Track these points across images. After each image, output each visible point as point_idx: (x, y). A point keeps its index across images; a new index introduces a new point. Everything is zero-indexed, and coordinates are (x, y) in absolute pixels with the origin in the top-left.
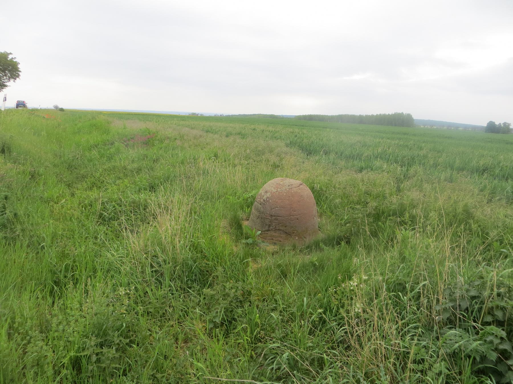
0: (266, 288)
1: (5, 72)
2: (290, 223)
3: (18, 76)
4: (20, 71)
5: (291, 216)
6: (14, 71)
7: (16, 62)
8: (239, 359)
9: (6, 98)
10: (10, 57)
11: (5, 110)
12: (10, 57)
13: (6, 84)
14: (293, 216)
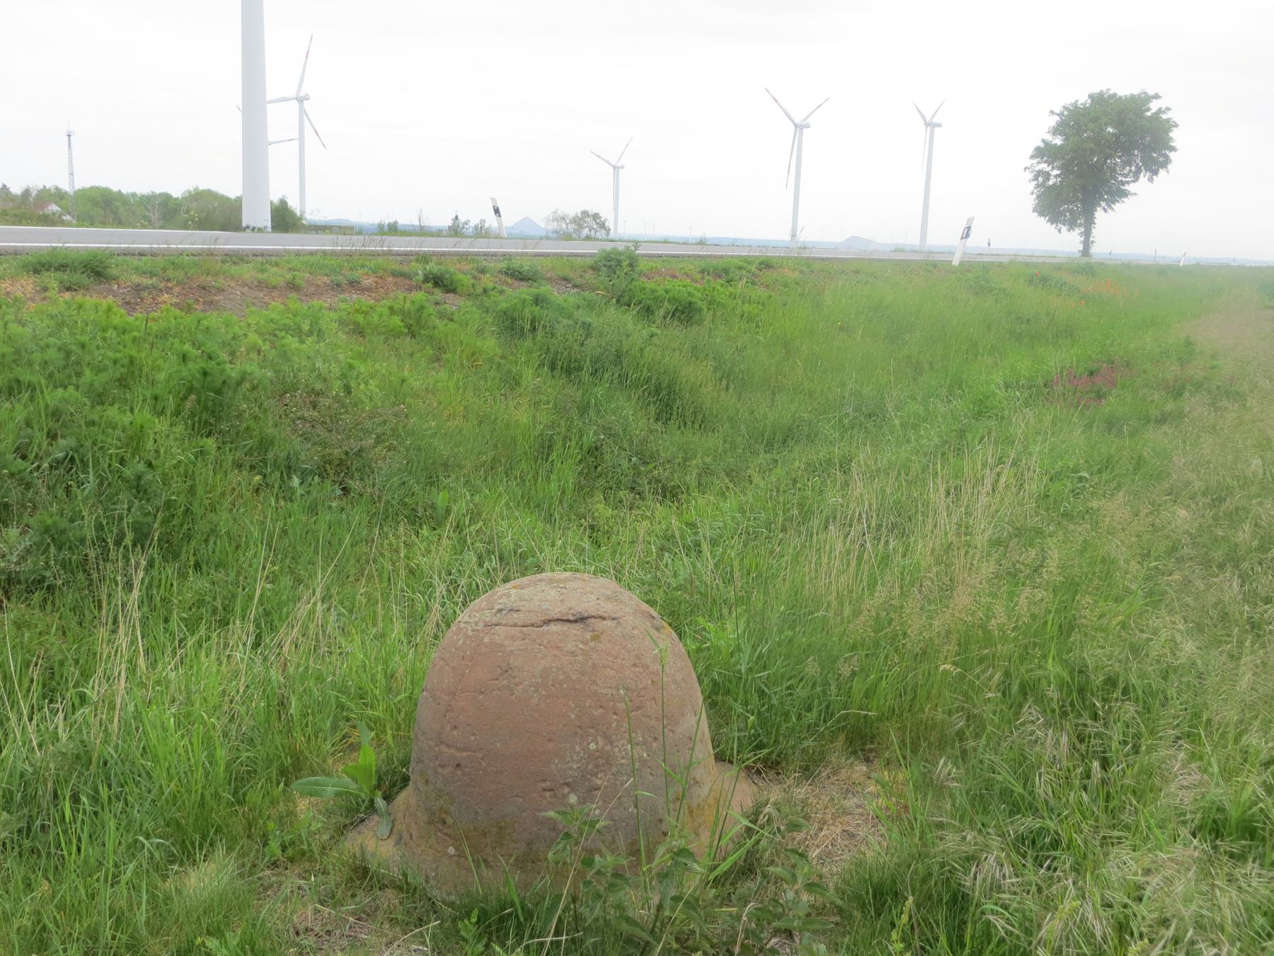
0: (262, 943)
3: (1165, 163)
4: (1173, 149)
7: (1168, 121)
9: (969, 228)
10: (1154, 106)
11: (961, 263)
12: (1154, 106)
13: (1127, 187)
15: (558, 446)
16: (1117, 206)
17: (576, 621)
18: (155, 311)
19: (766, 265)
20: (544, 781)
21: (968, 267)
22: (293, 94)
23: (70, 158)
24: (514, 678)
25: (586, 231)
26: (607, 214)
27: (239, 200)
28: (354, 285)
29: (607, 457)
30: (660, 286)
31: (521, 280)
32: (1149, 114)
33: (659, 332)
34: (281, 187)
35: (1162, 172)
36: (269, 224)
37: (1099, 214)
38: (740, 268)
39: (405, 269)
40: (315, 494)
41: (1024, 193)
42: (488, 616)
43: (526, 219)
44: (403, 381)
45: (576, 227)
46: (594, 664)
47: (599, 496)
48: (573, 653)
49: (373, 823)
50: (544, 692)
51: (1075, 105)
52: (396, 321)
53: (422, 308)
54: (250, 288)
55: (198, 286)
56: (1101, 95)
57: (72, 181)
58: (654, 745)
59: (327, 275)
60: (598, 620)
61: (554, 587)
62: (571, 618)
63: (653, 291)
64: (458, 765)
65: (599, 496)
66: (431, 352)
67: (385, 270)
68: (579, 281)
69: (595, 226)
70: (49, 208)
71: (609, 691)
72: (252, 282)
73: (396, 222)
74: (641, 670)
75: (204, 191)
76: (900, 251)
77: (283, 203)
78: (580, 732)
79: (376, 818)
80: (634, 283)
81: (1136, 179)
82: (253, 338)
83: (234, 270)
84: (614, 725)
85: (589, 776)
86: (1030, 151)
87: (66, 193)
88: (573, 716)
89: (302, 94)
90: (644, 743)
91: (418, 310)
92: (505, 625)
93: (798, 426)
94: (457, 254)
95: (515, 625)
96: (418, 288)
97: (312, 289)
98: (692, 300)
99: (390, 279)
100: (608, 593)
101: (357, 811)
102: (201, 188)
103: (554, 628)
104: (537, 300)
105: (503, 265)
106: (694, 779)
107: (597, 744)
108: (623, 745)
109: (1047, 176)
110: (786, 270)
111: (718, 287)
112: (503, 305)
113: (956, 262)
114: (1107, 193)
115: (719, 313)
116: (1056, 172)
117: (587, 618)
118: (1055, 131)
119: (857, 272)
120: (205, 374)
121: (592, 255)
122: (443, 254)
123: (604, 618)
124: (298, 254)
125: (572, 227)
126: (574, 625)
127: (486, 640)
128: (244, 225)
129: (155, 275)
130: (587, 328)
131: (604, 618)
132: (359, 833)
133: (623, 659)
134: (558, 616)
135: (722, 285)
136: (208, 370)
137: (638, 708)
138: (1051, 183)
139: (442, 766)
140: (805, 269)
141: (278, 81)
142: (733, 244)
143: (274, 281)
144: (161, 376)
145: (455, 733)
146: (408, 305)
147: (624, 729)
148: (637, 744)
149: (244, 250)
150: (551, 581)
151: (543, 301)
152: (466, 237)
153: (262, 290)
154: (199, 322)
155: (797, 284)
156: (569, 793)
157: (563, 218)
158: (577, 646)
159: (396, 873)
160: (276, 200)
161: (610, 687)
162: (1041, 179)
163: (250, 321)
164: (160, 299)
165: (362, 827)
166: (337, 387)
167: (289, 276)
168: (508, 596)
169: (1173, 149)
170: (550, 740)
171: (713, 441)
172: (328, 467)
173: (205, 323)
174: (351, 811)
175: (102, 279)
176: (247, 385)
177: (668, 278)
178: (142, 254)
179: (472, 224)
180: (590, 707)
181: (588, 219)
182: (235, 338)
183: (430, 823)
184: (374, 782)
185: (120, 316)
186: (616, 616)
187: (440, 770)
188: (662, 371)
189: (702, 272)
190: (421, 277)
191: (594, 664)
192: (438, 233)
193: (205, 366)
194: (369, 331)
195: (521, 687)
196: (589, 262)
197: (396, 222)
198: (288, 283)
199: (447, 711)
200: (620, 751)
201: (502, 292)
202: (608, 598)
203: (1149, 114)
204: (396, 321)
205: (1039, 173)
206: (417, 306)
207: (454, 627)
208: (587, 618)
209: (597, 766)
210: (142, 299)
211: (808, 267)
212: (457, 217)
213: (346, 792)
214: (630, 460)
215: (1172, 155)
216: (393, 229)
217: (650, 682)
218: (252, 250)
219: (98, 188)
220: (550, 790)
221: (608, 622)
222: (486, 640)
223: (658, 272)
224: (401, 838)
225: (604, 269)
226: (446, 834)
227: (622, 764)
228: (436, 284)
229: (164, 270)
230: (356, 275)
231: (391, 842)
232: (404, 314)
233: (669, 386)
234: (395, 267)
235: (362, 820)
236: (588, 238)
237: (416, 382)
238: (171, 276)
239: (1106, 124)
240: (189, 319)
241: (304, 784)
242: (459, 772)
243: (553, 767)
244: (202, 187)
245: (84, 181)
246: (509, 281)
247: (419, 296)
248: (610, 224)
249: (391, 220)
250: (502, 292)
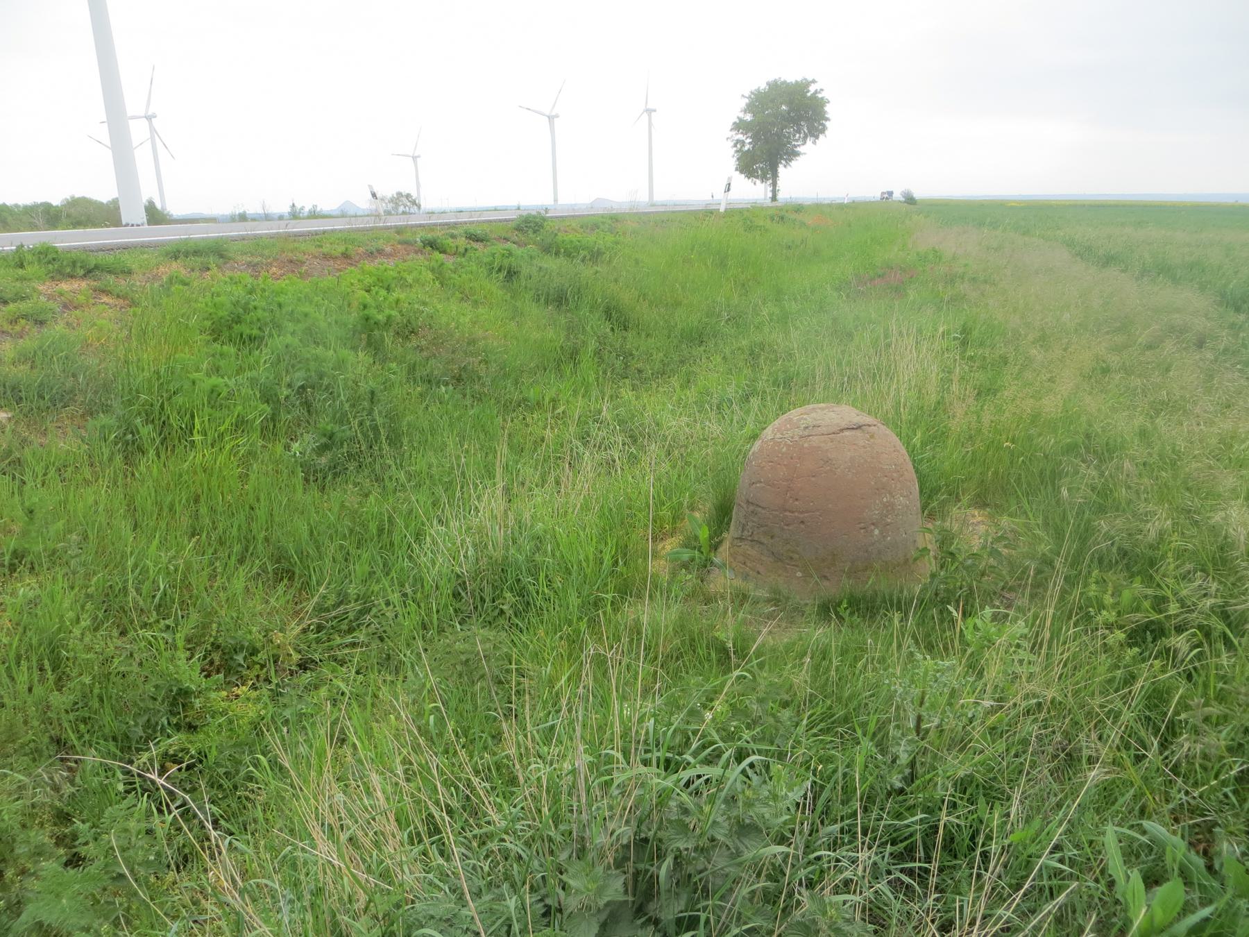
1: (799, 125)
2: (783, 529)
3: (823, 131)
4: (827, 119)
5: (785, 511)
6: (815, 120)
7: (822, 98)
8: (1084, 761)
10: (812, 89)
12: (812, 89)
13: (798, 149)
14: (793, 512)
16: (793, 163)
22: (143, 114)
25: (401, 209)
27: (115, 202)
28: (380, 252)
32: (809, 94)
34: (148, 191)
35: (821, 136)
36: (145, 220)
37: (781, 169)
41: (727, 161)
51: (758, 90)
53: (442, 264)
56: (775, 81)
81: (805, 143)
86: (730, 126)
89: (150, 113)
102: (77, 196)
103: (847, 433)
109: (743, 143)
113: (722, 210)
114: (785, 154)
116: (749, 140)
118: (745, 111)
125: (390, 206)
128: (124, 223)
131: (869, 426)
138: (746, 148)
141: (133, 104)
142: (472, 212)
145: (797, 503)
152: (300, 219)
162: (739, 146)
169: (827, 119)
179: (307, 209)
196: (513, 224)
198: (342, 254)
203: (809, 94)
205: (738, 141)
206: (439, 263)
212: (293, 205)
215: (827, 124)
216: (243, 218)
239: (781, 104)
242: (802, 526)
249: (241, 211)
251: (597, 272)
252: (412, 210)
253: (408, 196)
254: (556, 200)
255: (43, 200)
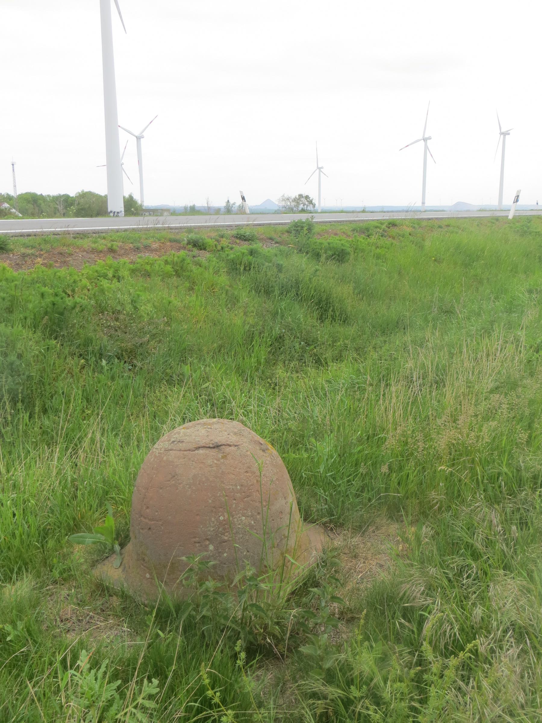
9: (518, 196)
11: (514, 217)
15: (256, 338)
17: (214, 448)
18: (33, 268)
19: (393, 224)
20: (195, 537)
21: (517, 219)
23: (14, 177)
24: (178, 480)
25: (301, 206)
26: (314, 196)
27: (106, 196)
28: (147, 248)
29: (287, 342)
30: (324, 241)
31: (245, 240)
33: (320, 268)
36: (123, 210)
38: (377, 227)
39: (178, 237)
40: (115, 369)
42: (167, 445)
43: (268, 200)
44: (170, 303)
45: (295, 204)
46: (222, 472)
47: (281, 364)
48: (211, 466)
49: (112, 559)
50: (194, 488)
52: (169, 268)
54: (87, 252)
55: (58, 253)
57: (16, 192)
58: (258, 517)
59: (132, 243)
60: (227, 447)
61: (205, 428)
62: (211, 446)
63: (321, 244)
64: (150, 529)
65: (281, 364)
66: (188, 285)
67: (165, 239)
68: (279, 240)
69: (307, 203)
70: (4, 205)
71: (231, 487)
72: (89, 249)
73: (194, 206)
74: (250, 475)
75: (87, 192)
76: (485, 210)
77: (131, 197)
78: (214, 510)
79: (115, 556)
80: (310, 240)
82: (85, 282)
83: (80, 242)
84: (234, 506)
85: (220, 535)
87: (13, 196)
88: (210, 501)
90: (252, 516)
91: (181, 261)
92: (175, 450)
93: (402, 320)
94: (208, 227)
95: (180, 450)
96: (184, 248)
97: (123, 251)
98: (344, 248)
99: (168, 244)
100: (236, 430)
101: (104, 552)
103: (201, 451)
104: (252, 253)
105: (234, 232)
106: (284, 535)
107: (224, 516)
108: (239, 517)
110: (405, 227)
111: (361, 240)
112: (232, 256)
113: (510, 217)
115: (360, 255)
117: (220, 446)
119: (448, 226)
120: (54, 304)
121: (285, 224)
122: (200, 227)
123: (230, 446)
124: (117, 231)
125: (293, 204)
126: (213, 450)
127: (165, 458)
128: (109, 210)
129: (34, 248)
130: (280, 268)
132: (104, 565)
133: (240, 469)
134: (204, 445)
135: (364, 238)
136: (55, 302)
137: (248, 496)
139: (142, 529)
140: (416, 226)
143: (100, 248)
144: (30, 306)
145: (148, 510)
146: (176, 259)
147: (239, 508)
148: (248, 517)
149: (87, 230)
150: (205, 424)
151: (255, 253)
153: (94, 254)
154: (55, 274)
155: (410, 235)
156: (209, 544)
157: (288, 199)
158: (213, 461)
159: (118, 588)
160: (127, 196)
161: (232, 485)
163: (83, 272)
164: (36, 261)
165: (106, 561)
166: (129, 308)
167: (109, 245)
168: (179, 433)
170: (198, 515)
171: (351, 330)
172: (124, 353)
173: (58, 274)
174: (101, 552)
175: (4, 251)
176: (77, 309)
177: (332, 235)
178: (29, 235)
180: (220, 496)
181: (302, 199)
182: (75, 282)
183: (138, 560)
184: (114, 536)
185: (11, 273)
186: (238, 444)
187: (141, 531)
188: (323, 290)
189: (353, 230)
190: (186, 242)
191: (222, 472)
192: (218, 211)
193: (53, 300)
194: (153, 274)
195: (181, 485)
196: (286, 227)
197: (194, 206)
199: (144, 498)
200: (238, 521)
201: (232, 249)
202: (235, 434)
204: (169, 268)
206: (180, 259)
207: (151, 451)
208: (220, 446)
209: (224, 529)
210: (26, 262)
211: (418, 224)
212: (228, 201)
213: (98, 542)
214: (300, 344)
217: (255, 481)
218: (92, 230)
219: (30, 193)
220: (199, 543)
221: (232, 448)
222: (165, 458)
223: (327, 232)
224: (125, 567)
225: (293, 232)
226: (145, 566)
227: (239, 528)
228: (195, 245)
229: (40, 244)
230: (148, 242)
231: (120, 570)
232: (174, 264)
233: (327, 299)
234: (172, 236)
235: (107, 557)
236: (303, 211)
237: (176, 302)
238: (43, 247)
240: (50, 272)
241: (75, 537)
243: (199, 530)
244: (86, 190)
245: (22, 189)
246: (238, 241)
247: (182, 253)
248: (316, 201)
249: (192, 205)
250: (232, 249)
251: (316, 271)
252: (309, 208)
253: (307, 197)
254: (423, 203)
255: (48, 194)
